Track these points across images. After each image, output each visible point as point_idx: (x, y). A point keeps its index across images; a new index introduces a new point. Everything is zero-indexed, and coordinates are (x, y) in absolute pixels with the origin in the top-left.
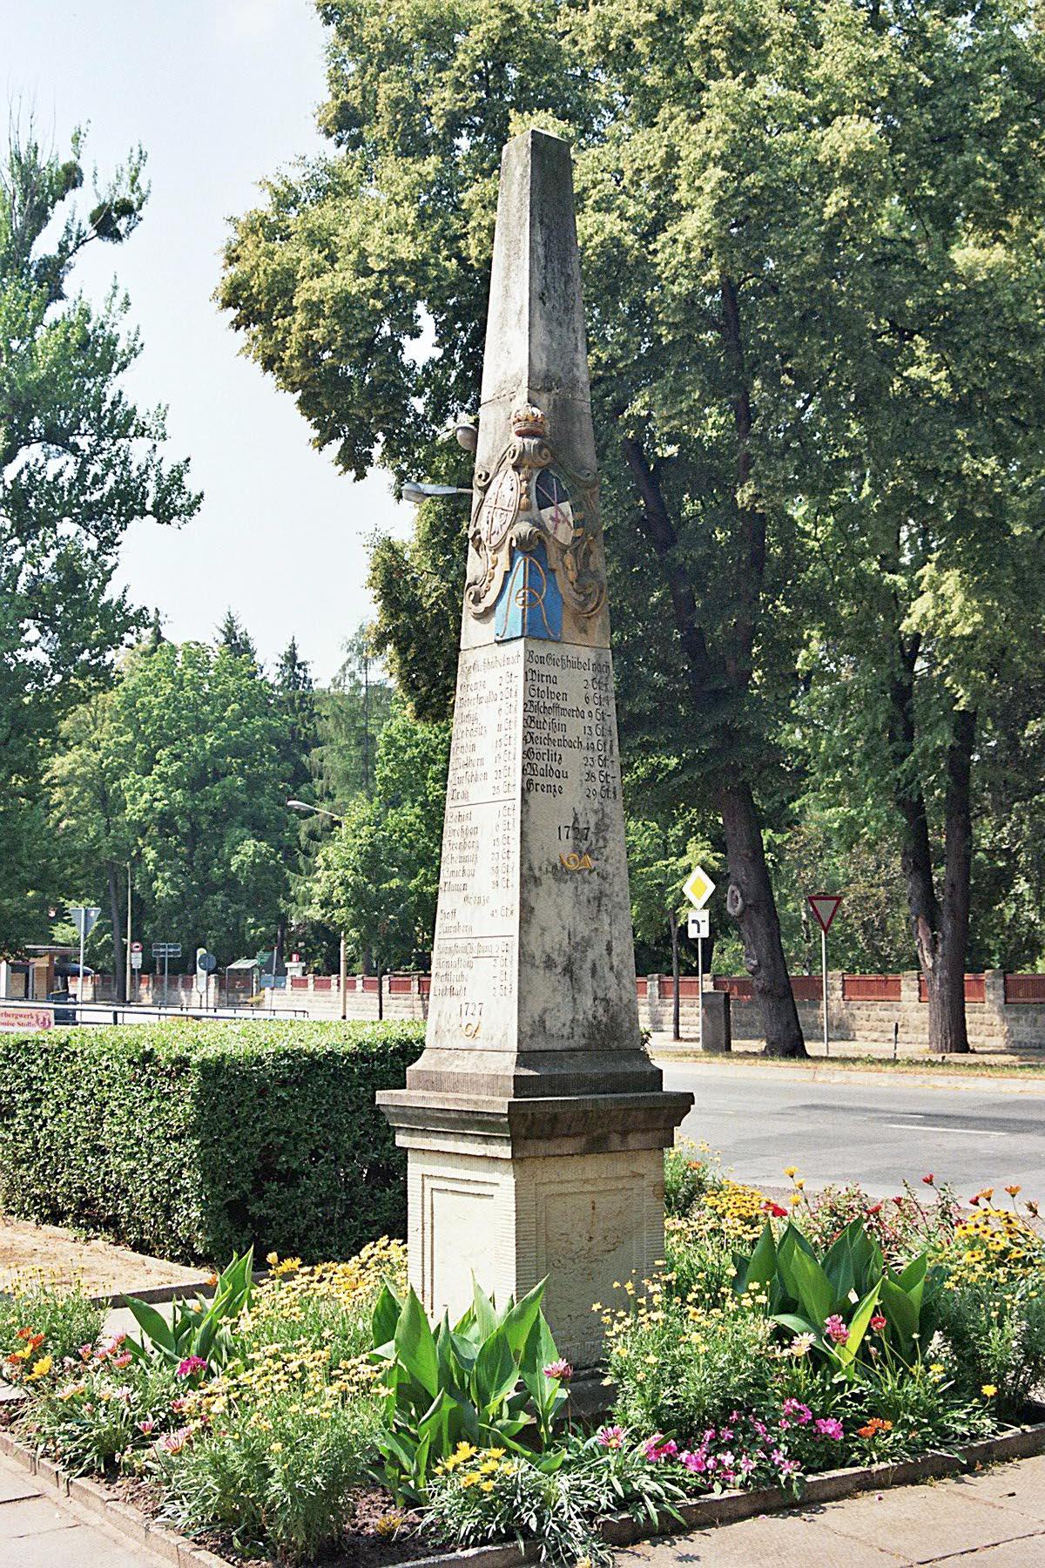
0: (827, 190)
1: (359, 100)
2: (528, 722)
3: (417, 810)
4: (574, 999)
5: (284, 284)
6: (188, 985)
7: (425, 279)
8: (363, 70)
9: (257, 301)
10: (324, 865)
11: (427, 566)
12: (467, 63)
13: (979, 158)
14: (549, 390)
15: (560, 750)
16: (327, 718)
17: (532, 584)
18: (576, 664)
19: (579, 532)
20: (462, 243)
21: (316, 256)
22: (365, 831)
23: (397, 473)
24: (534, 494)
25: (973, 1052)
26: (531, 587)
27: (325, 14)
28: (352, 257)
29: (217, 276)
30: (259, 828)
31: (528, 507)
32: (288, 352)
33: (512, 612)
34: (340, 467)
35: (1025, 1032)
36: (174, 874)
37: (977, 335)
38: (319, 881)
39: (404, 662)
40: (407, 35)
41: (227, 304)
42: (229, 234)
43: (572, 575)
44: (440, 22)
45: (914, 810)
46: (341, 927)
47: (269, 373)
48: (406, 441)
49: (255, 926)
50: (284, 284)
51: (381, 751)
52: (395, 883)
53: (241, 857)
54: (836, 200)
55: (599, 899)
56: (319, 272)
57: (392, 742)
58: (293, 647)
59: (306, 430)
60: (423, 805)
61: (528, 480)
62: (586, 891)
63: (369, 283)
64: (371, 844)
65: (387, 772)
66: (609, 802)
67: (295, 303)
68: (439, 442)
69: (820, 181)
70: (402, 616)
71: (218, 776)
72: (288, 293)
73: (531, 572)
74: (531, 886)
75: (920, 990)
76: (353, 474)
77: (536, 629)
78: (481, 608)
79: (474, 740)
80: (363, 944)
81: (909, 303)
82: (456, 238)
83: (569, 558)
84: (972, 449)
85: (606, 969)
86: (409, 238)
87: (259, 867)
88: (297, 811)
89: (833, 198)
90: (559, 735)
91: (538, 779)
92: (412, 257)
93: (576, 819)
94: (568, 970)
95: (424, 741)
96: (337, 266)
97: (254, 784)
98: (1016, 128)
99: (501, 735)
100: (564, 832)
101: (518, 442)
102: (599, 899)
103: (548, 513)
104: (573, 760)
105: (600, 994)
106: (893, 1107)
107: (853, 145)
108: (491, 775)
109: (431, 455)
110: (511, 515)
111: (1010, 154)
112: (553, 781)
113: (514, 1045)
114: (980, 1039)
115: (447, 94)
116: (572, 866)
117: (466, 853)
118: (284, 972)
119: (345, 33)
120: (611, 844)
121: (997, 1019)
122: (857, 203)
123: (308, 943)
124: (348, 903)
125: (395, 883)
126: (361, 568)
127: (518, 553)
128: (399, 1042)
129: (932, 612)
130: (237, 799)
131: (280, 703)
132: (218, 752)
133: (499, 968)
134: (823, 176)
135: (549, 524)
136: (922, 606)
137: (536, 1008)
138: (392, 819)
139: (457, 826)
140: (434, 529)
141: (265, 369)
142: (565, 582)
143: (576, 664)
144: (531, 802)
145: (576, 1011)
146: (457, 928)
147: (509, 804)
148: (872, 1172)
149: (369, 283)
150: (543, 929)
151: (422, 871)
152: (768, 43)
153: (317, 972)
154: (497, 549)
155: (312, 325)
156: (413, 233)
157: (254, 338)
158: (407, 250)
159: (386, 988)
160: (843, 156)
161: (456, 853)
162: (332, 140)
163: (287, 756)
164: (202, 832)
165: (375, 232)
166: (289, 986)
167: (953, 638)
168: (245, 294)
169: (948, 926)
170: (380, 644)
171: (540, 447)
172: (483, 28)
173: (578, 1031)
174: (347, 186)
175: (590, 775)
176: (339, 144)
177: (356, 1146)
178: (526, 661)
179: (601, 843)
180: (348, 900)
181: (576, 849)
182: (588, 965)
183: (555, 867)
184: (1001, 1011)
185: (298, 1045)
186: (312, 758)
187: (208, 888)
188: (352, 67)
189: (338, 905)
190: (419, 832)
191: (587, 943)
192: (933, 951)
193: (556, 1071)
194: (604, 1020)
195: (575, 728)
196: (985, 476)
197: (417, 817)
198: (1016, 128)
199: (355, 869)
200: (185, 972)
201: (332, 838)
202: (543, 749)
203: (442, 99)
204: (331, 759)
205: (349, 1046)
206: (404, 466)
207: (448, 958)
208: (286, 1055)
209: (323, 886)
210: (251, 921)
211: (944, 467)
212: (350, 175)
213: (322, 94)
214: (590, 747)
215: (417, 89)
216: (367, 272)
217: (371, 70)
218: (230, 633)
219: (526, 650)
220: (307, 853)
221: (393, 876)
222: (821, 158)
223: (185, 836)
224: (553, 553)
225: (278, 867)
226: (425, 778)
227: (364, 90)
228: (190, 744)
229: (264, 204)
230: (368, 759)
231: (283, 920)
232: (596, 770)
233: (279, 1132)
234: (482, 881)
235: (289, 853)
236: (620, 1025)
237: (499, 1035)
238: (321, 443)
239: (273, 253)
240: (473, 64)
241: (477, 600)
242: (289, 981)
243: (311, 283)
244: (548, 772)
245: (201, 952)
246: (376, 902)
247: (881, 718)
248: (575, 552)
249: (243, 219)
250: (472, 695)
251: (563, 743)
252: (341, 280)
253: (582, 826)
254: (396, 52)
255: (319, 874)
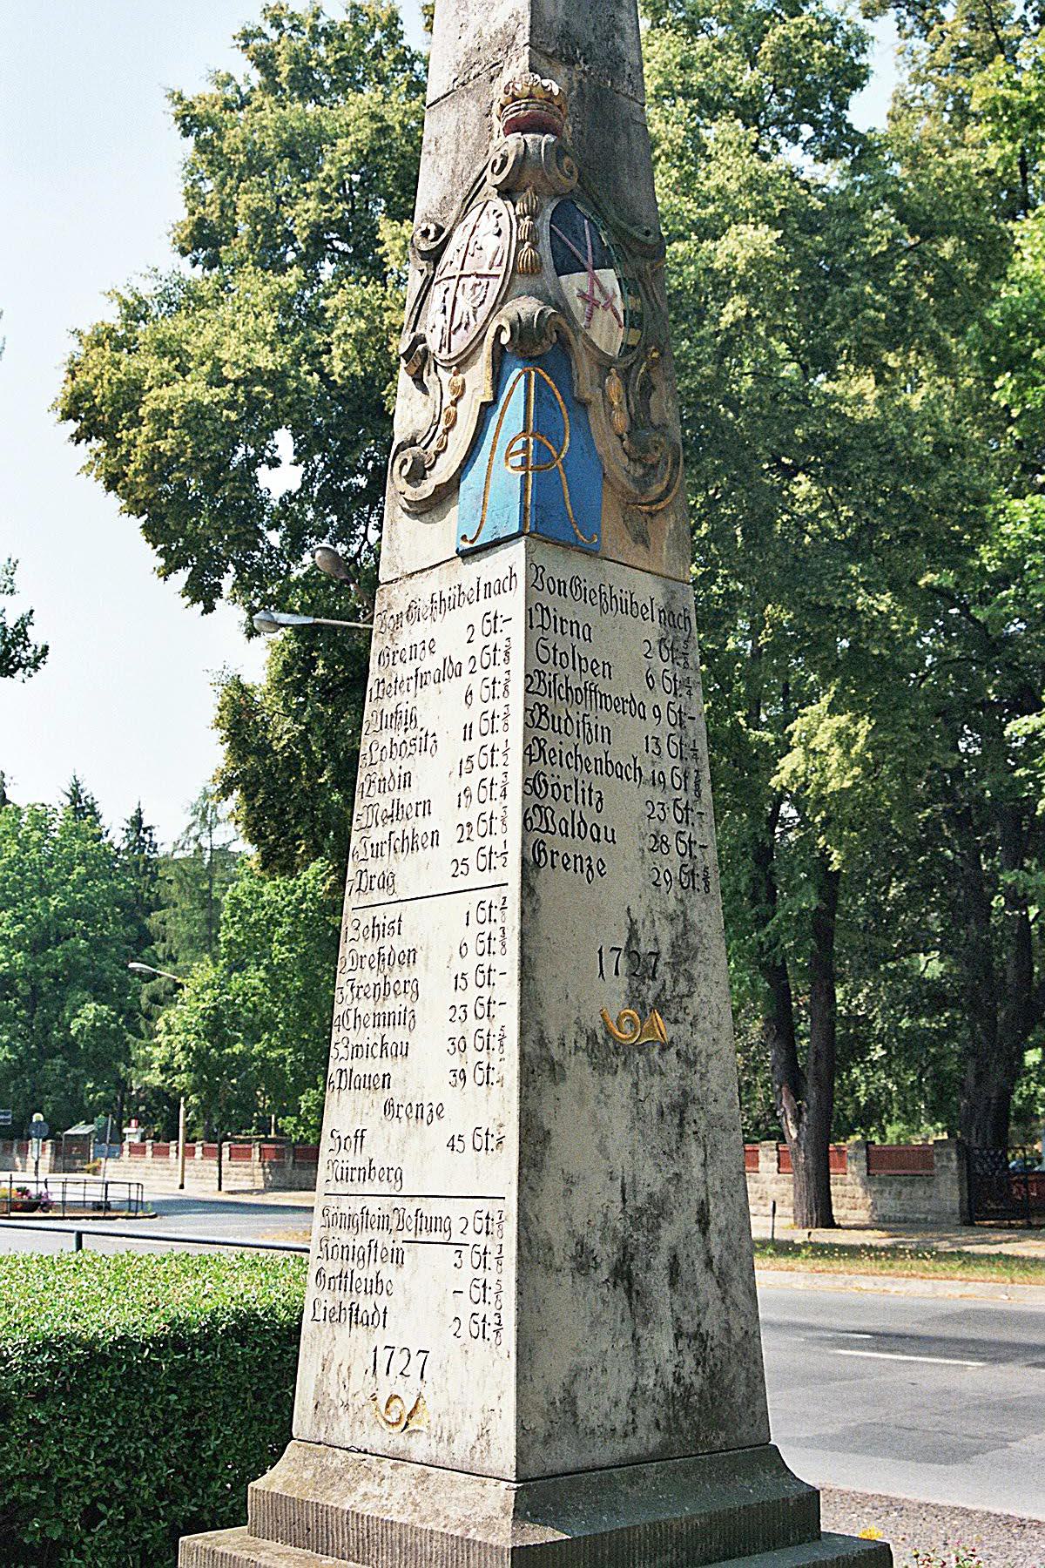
0: (723, 300)
1: (217, 214)
2: (535, 716)
3: (262, 974)
4: (636, 1339)
5: (130, 395)
6: (23, 1151)
7: (284, 392)
8: (223, 183)
9: (100, 413)
10: (165, 1029)
11: (279, 707)
12: (334, 173)
13: (868, 289)
14: (571, 62)
15: (599, 782)
16: (170, 882)
17: (541, 425)
18: (630, 607)
19: (635, 337)
20: (325, 358)
21: (165, 364)
22: (209, 993)
23: (248, 610)
24: (546, 241)
25: (839, 1227)
26: (539, 431)
27: (184, 126)
28: (205, 369)
29: (56, 387)
30: (100, 991)
31: (534, 269)
32: (132, 466)
33: (498, 488)
34: (188, 600)
35: (890, 1205)
36: (13, 1038)
37: (868, 469)
38: (159, 1045)
39: (251, 809)
40: (271, 149)
41: (67, 415)
42: (73, 347)
43: (621, 421)
44: (306, 134)
45: (777, 974)
46: (182, 1093)
47: (113, 493)
48: (258, 572)
49: (94, 1091)
50: (130, 395)
51: (225, 914)
52: (238, 1048)
53: (81, 1021)
54: (733, 309)
55: (680, 1109)
56: (166, 380)
57: (237, 903)
58: (139, 811)
59: (151, 558)
60: (267, 968)
61: (534, 215)
62: (658, 1091)
63: (224, 393)
64: (215, 1008)
65: (232, 934)
66: (696, 897)
67: (141, 412)
68: (293, 577)
69: (715, 291)
70: (251, 760)
71: (62, 937)
72: (133, 405)
73: (541, 402)
74: (543, 1080)
75: (779, 1160)
76: (200, 606)
77: (549, 523)
78: (427, 488)
79: (408, 765)
80: (204, 1110)
81: (799, 432)
82: (318, 354)
83: (614, 385)
84: (865, 585)
85: (699, 1266)
86: (268, 348)
87: (99, 1031)
88: (140, 975)
89: (730, 307)
90: (595, 751)
91: (555, 842)
92: (271, 366)
93: (633, 935)
94: (623, 1274)
95: (270, 903)
96: (188, 378)
97: (97, 946)
98: (904, 262)
99: (472, 747)
100: (610, 959)
101: (512, 144)
102: (680, 1109)
103: (574, 284)
104: (625, 805)
105: (689, 1327)
106: (837, 1322)
107: (752, 252)
108: (449, 835)
109: (285, 591)
110: (495, 285)
111: (897, 288)
112: (588, 848)
113: (504, 1457)
114: (842, 1212)
115: (311, 204)
116: (625, 1035)
117: (393, 1004)
118: (122, 1138)
119: (202, 147)
120: (702, 989)
121: (860, 1191)
122: (755, 313)
123: (149, 1108)
124: (189, 1069)
125: (238, 1048)
126: (209, 705)
127: (510, 360)
128: (236, 1315)
129: (803, 767)
130: (78, 962)
131: (125, 867)
132: (60, 915)
133: (467, 1273)
134: (720, 284)
135: (578, 306)
136: (792, 762)
137: (554, 1369)
138: (237, 980)
139: (369, 948)
140: (287, 669)
141: (108, 489)
142: (609, 425)
143: (630, 607)
144: (541, 891)
145: (639, 1368)
146: (368, 1173)
147: (491, 896)
148: (856, 1432)
149: (224, 393)
150: (570, 1181)
151: (266, 1036)
152: (657, 152)
153: (156, 1138)
154: (463, 362)
155: (159, 435)
156: (272, 343)
157: (97, 455)
158: (265, 359)
159: (226, 1156)
160: (741, 265)
161: (366, 1007)
162: (187, 259)
163: (131, 919)
164: (43, 995)
165: (232, 340)
166: (126, 1153)
167: (824, 797)
168: (87, 405)
169: (812, 1094)
170: (226, 791)
171: (558, 151)
172: (352, 139)
173: (646, 1414)
174: (201, 301)
175: (659, 840)
176: (195, 263)
177: (161, 1493)
178: (530, 586)
179: (683, 987)
180: (189, 1065)
181: (635, 998)
182: (661, 1260)
183: (592, 1038)
184: (864, 1184)
185: (68, 1326)
186: (153, 921)
187: (47, 1052)
188: (209, 185)
189: (178, 1071)
190: (263, 995)
191: (655, 1212)
192: (797, 1120)
193: (607, 1523)
194: (697, 1381)
195: (630, 739)
196: (881, 613)
197: (262, 980)
198: (904, 262)
199: (196, 1033)
200: (21, 1137)
201: (175, 1002)
202: (566, 777)
203: (304, 214)
204: (174, 922)
205: (155, 1325)
206: (256, 603)
207: (345, 1237)
208: (47, 1345)
209: (166, 1046)
210: (90, 1085)
211: (838, 603)
212: (206, 291)
213: (180, 213)
214: (657, 781)
215: (279, 201)
216: (222, 382)
217: (231, 182)
218: (75, 796)
219: (530, 563)
220: (149, 1017)
221: (236, 1040)
222: (717, 265)
223: (24, 998)
224: (584, 369)
225: (119, 1030)
226: (270, 940)
227: (223, 204)
228: (33, 906)
229: (112, 316)
230: (213, 922)
231: (123, 1085)
232: (669, 828)
233: (31, 1478)
234: (425, 1071)
235: (131, 1015)
236: (728, 1392)
237: (469, 1433)
238: (166, 573)
239: (119, 363)
240: (341, 175)
241: (417, 474)
242: (126, 1147)
243: (161, 392)
244: (580, 828)
245: (37, 1117)
246: (218, 1068)
247: (744, 880)
248: (625, 374)
249: (88, 332)
250: (405, 670)
251: (609, 767)
252: (195, 389)
253: (645, 947)
254: (256, 164)
255: (159, 1039)
